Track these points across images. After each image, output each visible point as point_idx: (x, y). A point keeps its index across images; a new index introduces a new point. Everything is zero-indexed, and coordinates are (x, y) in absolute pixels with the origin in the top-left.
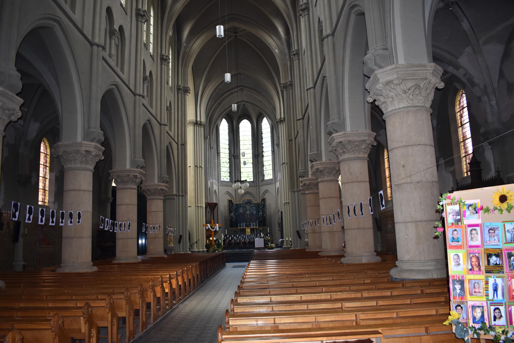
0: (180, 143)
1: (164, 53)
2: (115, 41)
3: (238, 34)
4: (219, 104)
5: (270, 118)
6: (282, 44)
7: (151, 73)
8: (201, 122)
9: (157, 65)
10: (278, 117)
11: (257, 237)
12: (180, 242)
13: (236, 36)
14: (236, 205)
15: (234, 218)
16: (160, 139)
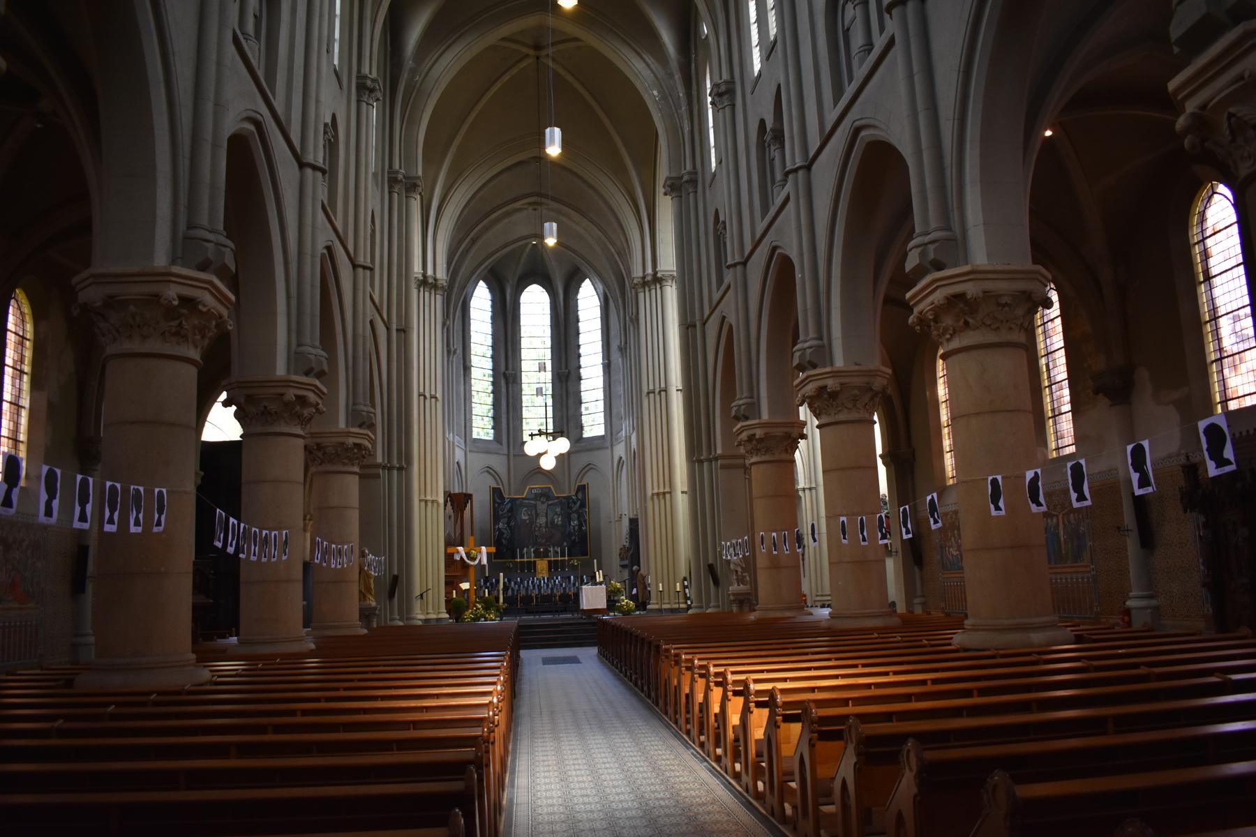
0: (394, 327)
3: (543, 53)
4: (474, 241)
5: (600, 278)
6: (671, 75)
8: (435, 279)
10: (637, 273)
11: (582, 583)
12: (391, 595)
13: (538, 58)
14: (513, 500)
15: (507, 533)
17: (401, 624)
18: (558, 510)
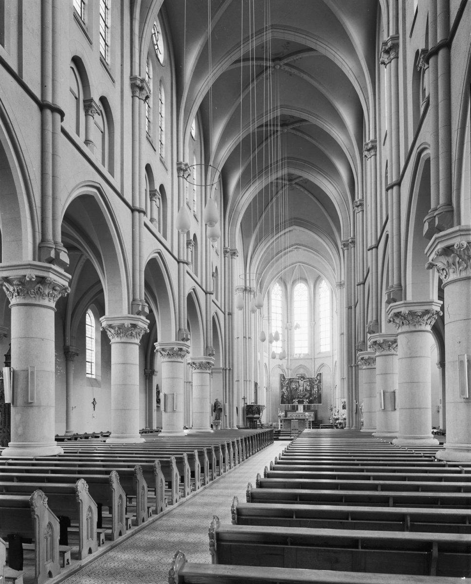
0: (227, 313)
1: (136, 73)
2: (157, 202)
7: (195, 236)
8: (250, 288)
9: (202, 226)
15: (286, 393)
16: (207, 308)
17: (230, 428)
18: (308, 383)
